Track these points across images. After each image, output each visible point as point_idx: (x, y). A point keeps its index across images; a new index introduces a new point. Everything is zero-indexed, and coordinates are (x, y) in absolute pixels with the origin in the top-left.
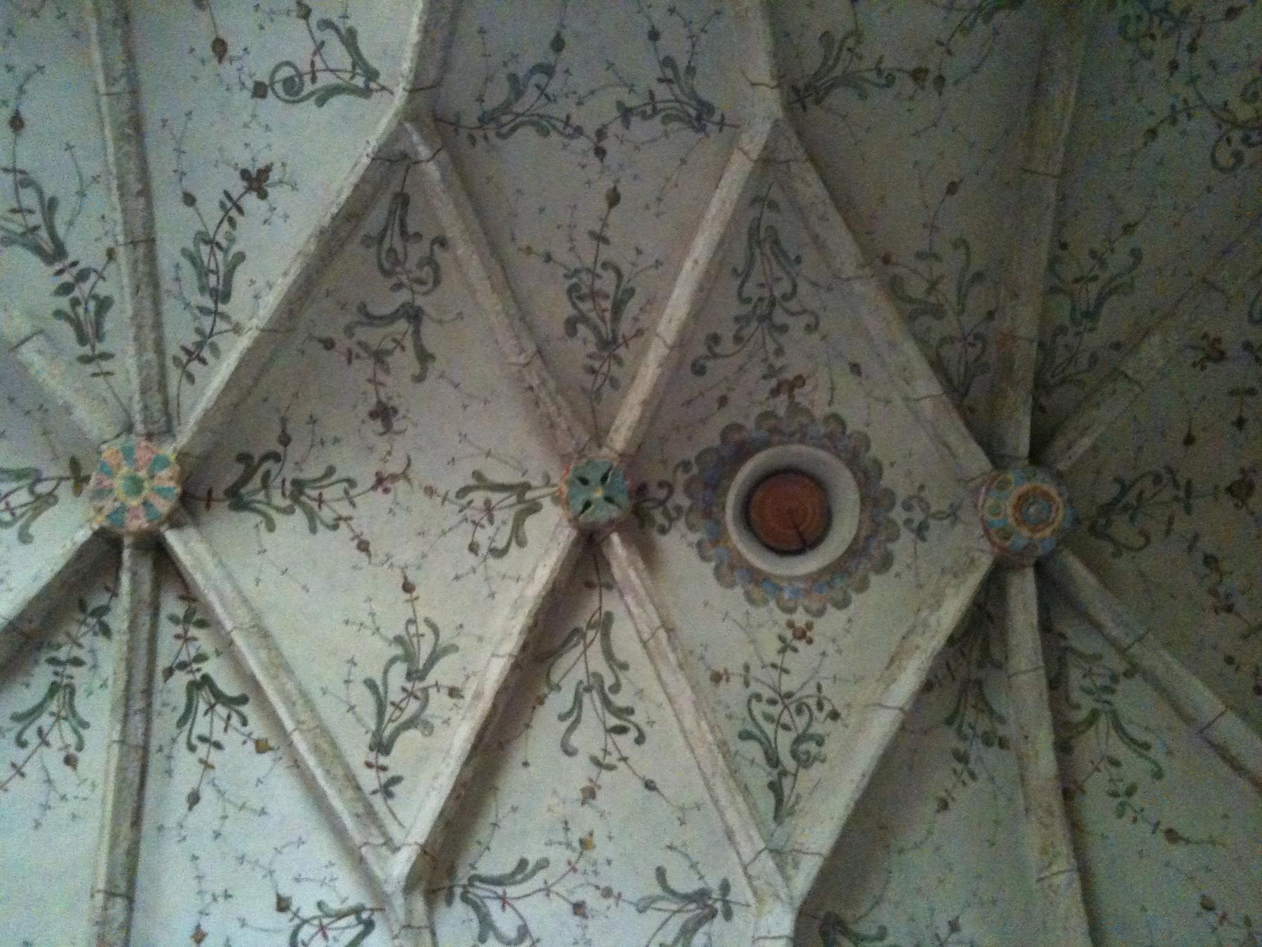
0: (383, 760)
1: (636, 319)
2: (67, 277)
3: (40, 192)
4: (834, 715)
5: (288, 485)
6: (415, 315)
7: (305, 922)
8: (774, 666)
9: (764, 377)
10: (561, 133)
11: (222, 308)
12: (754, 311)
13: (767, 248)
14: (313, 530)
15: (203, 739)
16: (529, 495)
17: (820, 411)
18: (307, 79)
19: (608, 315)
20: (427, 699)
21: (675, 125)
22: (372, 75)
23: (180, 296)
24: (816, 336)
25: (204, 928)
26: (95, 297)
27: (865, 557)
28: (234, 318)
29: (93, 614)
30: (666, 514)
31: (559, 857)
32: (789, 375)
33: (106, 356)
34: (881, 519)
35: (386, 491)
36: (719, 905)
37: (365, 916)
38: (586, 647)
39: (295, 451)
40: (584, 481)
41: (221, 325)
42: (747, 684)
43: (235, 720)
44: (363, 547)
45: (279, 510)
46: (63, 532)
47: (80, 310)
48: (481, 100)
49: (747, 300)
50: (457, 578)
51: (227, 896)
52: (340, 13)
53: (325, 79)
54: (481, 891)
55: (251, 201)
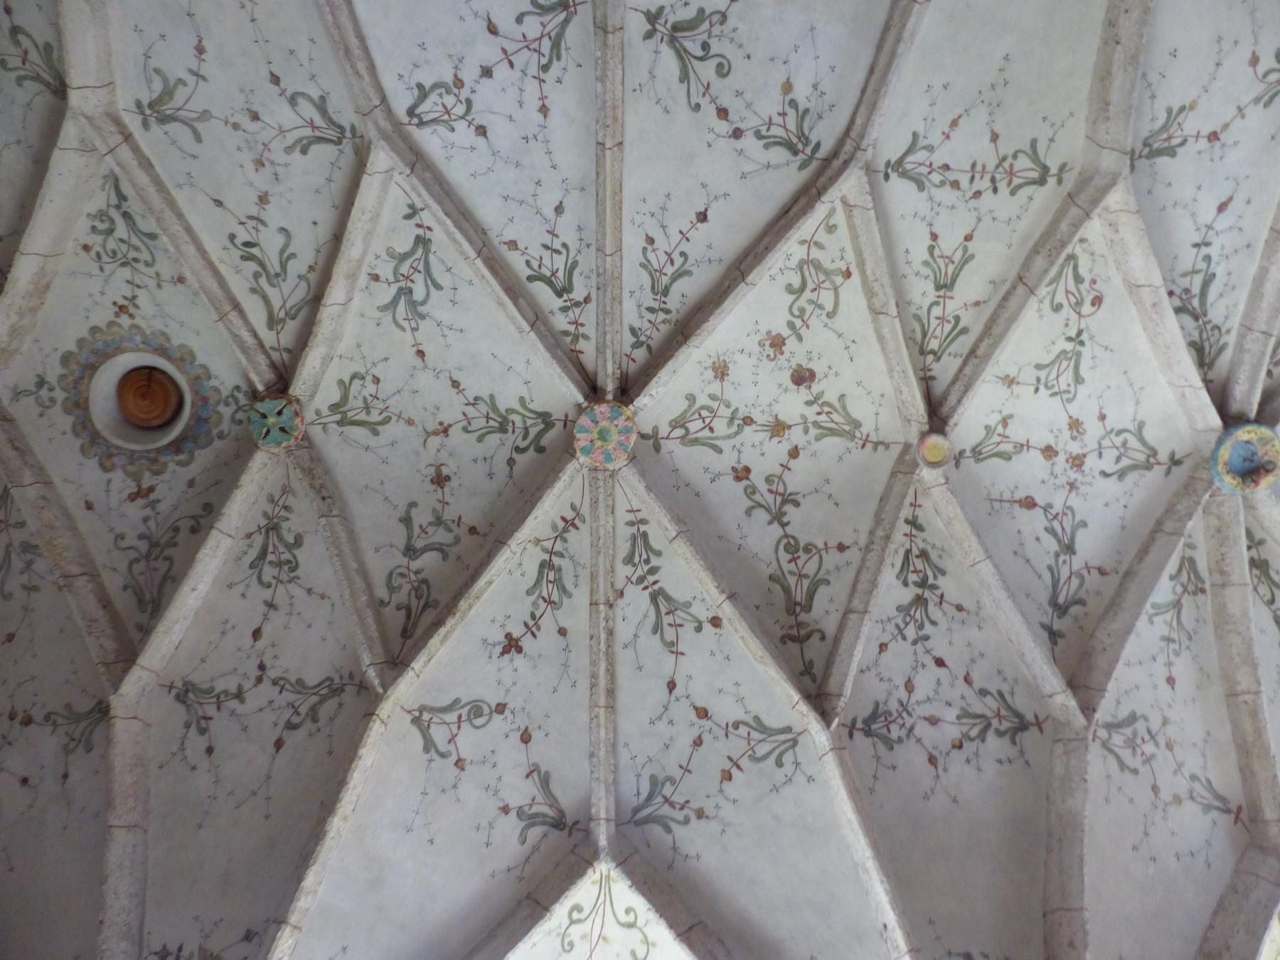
0: (420, 231)
1: (250, 546)
2: (651, 579)
3: (662, 638)
4: (86, 248)
5: (510, 429)
6: (411, 551)
7: (462, 118)
8: (139, 287)
9: (158, 501)
10: (288, 681)
11: (547, 557)
12: (162, 551)
13: (148, 596)
14: (492, 397)
15: (558, 252)
16: (338, 417)
17: (117, 476)
18: (464, 718)
19: (271, 549)
20: (395, 274)
21: (205, 686)
22: (416, 721)
23: (576, 564)
24: (118, 531)
25: (541, 116)
26: (634, 565)
27: (84, 364)
28: (538, 548)
29: (642, 344)
30: (236, 400)
31: (277, 154)
32: (140, 502)
33: (631, 524)
34: (73, 391)
35: (441, 424)
36: (148, 112)
37: (415, 121)
38: (284, 305)
39: (505, 453)
40: (282, 429)
41: (548, 545)
42: (158, 274)
43: (535, 265)
44: (455, 384)
45: (513, 411)
46: (659, 402)
47: (644, 556)
48: (340, 705)
49: (166, 559)
50: (386, 359)
51: (526, 139)
52: (433, 764)
53: (451, 717)
54: (332, 134)
55: (517, 631)
